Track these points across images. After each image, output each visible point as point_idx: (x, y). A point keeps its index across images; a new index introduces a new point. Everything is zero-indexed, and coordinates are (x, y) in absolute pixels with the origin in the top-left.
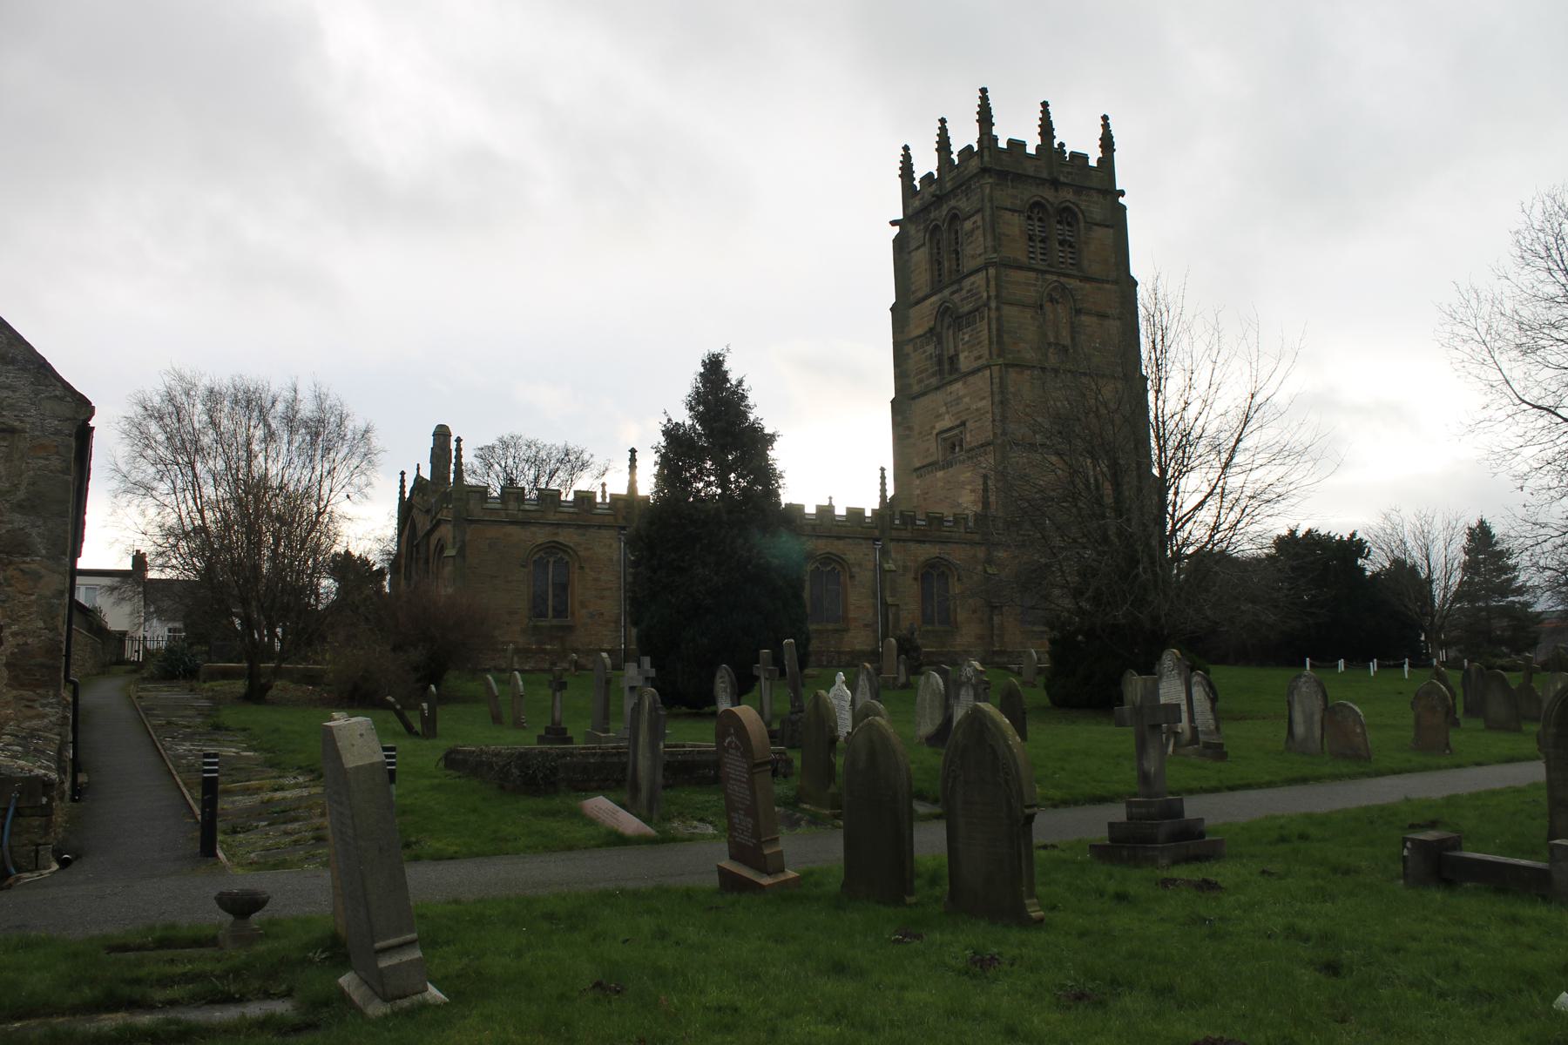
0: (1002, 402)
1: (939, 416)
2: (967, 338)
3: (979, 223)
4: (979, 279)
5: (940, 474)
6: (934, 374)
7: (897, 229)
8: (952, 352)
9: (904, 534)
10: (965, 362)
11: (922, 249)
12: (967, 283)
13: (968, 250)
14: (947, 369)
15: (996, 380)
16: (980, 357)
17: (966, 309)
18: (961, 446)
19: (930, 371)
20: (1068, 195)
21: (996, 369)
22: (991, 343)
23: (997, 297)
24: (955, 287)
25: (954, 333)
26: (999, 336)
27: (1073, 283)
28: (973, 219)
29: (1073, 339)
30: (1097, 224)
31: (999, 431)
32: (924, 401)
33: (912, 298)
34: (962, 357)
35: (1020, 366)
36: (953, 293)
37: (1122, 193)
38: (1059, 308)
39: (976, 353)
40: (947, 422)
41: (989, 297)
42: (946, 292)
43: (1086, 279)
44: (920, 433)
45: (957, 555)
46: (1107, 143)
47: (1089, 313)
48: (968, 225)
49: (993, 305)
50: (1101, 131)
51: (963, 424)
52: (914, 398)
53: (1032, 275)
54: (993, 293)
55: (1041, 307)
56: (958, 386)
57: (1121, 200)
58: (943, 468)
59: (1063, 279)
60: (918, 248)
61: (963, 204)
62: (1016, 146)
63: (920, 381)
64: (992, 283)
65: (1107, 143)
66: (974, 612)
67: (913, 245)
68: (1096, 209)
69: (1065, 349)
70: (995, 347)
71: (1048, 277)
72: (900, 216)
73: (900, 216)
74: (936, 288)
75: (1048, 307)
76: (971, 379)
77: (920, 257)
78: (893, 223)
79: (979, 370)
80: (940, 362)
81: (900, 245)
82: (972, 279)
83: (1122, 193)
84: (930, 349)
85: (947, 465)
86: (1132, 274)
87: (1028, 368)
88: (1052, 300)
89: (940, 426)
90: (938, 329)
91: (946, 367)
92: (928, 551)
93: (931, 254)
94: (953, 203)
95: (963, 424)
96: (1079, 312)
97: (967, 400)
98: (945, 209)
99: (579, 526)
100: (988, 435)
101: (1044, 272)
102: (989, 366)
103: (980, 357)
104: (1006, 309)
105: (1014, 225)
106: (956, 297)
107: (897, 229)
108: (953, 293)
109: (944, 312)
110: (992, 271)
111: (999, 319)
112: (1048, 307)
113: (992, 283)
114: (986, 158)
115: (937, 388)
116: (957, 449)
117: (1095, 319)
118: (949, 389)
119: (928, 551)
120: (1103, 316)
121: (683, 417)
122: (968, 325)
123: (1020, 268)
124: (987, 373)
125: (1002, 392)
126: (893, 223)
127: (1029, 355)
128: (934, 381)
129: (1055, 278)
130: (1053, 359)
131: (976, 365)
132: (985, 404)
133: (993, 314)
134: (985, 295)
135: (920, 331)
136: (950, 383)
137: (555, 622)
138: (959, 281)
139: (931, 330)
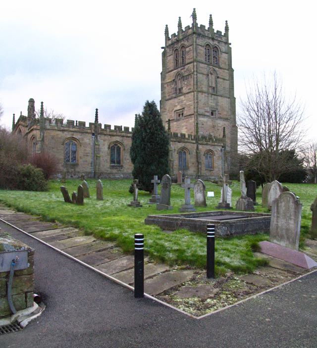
0: (197, 102)
1: (176, 106)
2: (186, 83)
3: (191, 49)
4: (191, 66)
5: (175, 123)
6: (174, 94)
7: (163, 50)
8: (180, 87)
9: (174, 140)
10: (185, 90)
11: (172, 56)
12: (186, 67)
13: (187, 57)
14: (179, 92)
15: (196, 96)
16: (190, 89)
17: (186, 74)
18: (183, 114)
19: (173, 92)
20: (216, 43)
21: (195, 92)
22: (194, 85)
23: (197, 71)
24: (182, 68)
25: (181, 81)
26: (197, 83)
27: (217, 69)
28: (189, 48)
29: (216, 85)
30: (224, 53)
31: (196, 111)
32: (171, 101)
33: (167, 71)
34: (184, 89)
35: (202, 92)
36: (182, 69)
37: (230, 44)
38: (213, 76)
39: (189, 88)
40: (178, 107)
41: (194, 71)
42: (179, 69)
43: (221, 68)
44: (169, 111)
45: (189, 146)
46: (227, 29)
47: (221, 78)
48: (187, 49)
49: (195, 73)
50: (225, 25)
51: (184, 108)
52: (167, 100)
53: (206, 65)
54: (195, 70)
55: (208, 75)
56: (182, 97)
57: (230, 46)
58: (176, 121)
59: (214, 68)
60: (170, 56)
61: (186, 43)
62: (202, 27)
63: (169, 96)
64: (195, 67)
65: (227, 29)
66: (193, 164)
67: (168, 55)
68: (223, 48)
69: (214, 88)
70: (195, 86)
71: (210, 66)
72: (164, 46)
73: (164, 46)
74: (176, 67)
75: (210, 75)
76: (187, 95)
77: (171, 59)
78: (162, 48)
79: (190, 92)
80: (176, 90)
81: (164, 54)
82: (188, 65)
83: (230, 44)
84: (173, 86)
85: (178, 120)
86: (233, 67)
87: (205, 93)
88: (211, 74)
89: (176, 109)
90: (176, 80)
91: (178, 91)
92: (180, 145)
93: (174, 58)
94: (182, 42)
95: (184, 108)
96: (218, 77)
97: (185, 101)
98: (180, 44)
99: (110, 135)
100: (192, 112)
101: (209, 65)
102: (193, 92)
103: (190, 89)
104: (199, 75)
105: (202, 50)
106: (183, 71)
107: (163, 50)
108: (182, 69)
109: (178, 74)
110: (195, 63)
111: (196, 78)
112: (210, 75)
113: (195, 67)
114: (195, 29)
115: (175, 97)
116: (181, 116)
117: (222, 80)
118: (179, 98)
119: (180, 145)
120: (224, 79)
121: (141, 114)
122: (187, 79)
123: (202, 63)
124: (193, 93)
125: (197, 99)
126: (162, 48)
127: (205, 89)
128: (174, 95)
129: (212, 67)
130: (211, 91)
131: (188, 91)
132: (192, 103)
133: (195, 76)
134: (193, 70)
135: (170, 81)
136: (180, 96)
137: (72, 163)
138: (184, 66)
139: (174, 80)
